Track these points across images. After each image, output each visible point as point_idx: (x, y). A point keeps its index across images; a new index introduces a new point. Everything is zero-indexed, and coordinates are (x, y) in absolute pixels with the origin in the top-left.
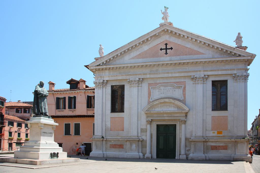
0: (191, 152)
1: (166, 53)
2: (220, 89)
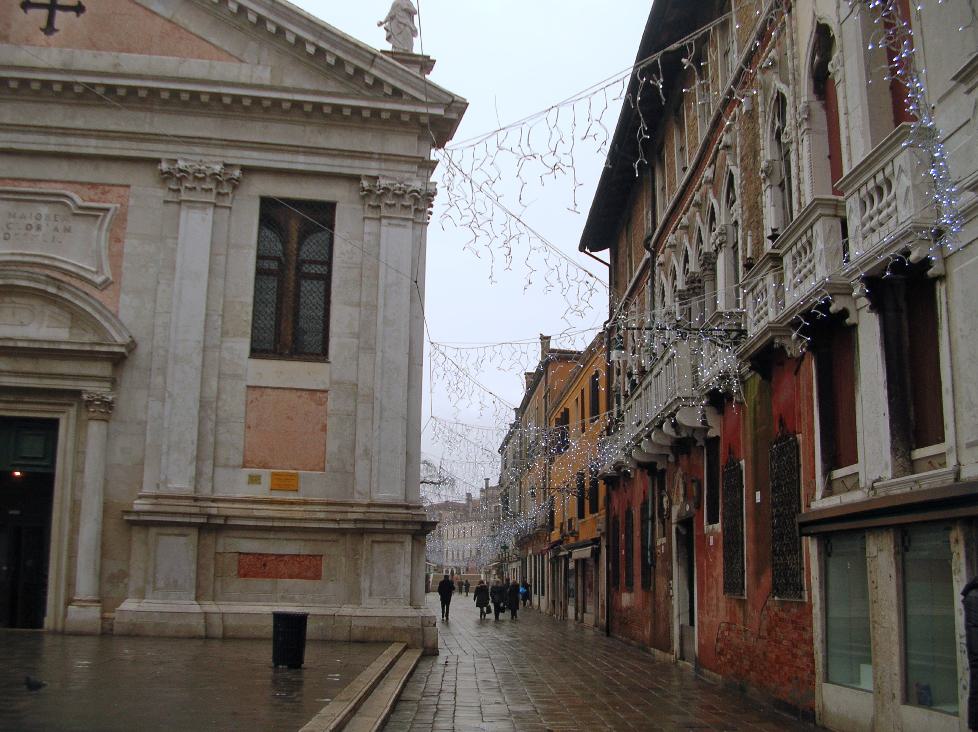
0: (132, 588)
1: (49, 28)
2: (300, 243)
